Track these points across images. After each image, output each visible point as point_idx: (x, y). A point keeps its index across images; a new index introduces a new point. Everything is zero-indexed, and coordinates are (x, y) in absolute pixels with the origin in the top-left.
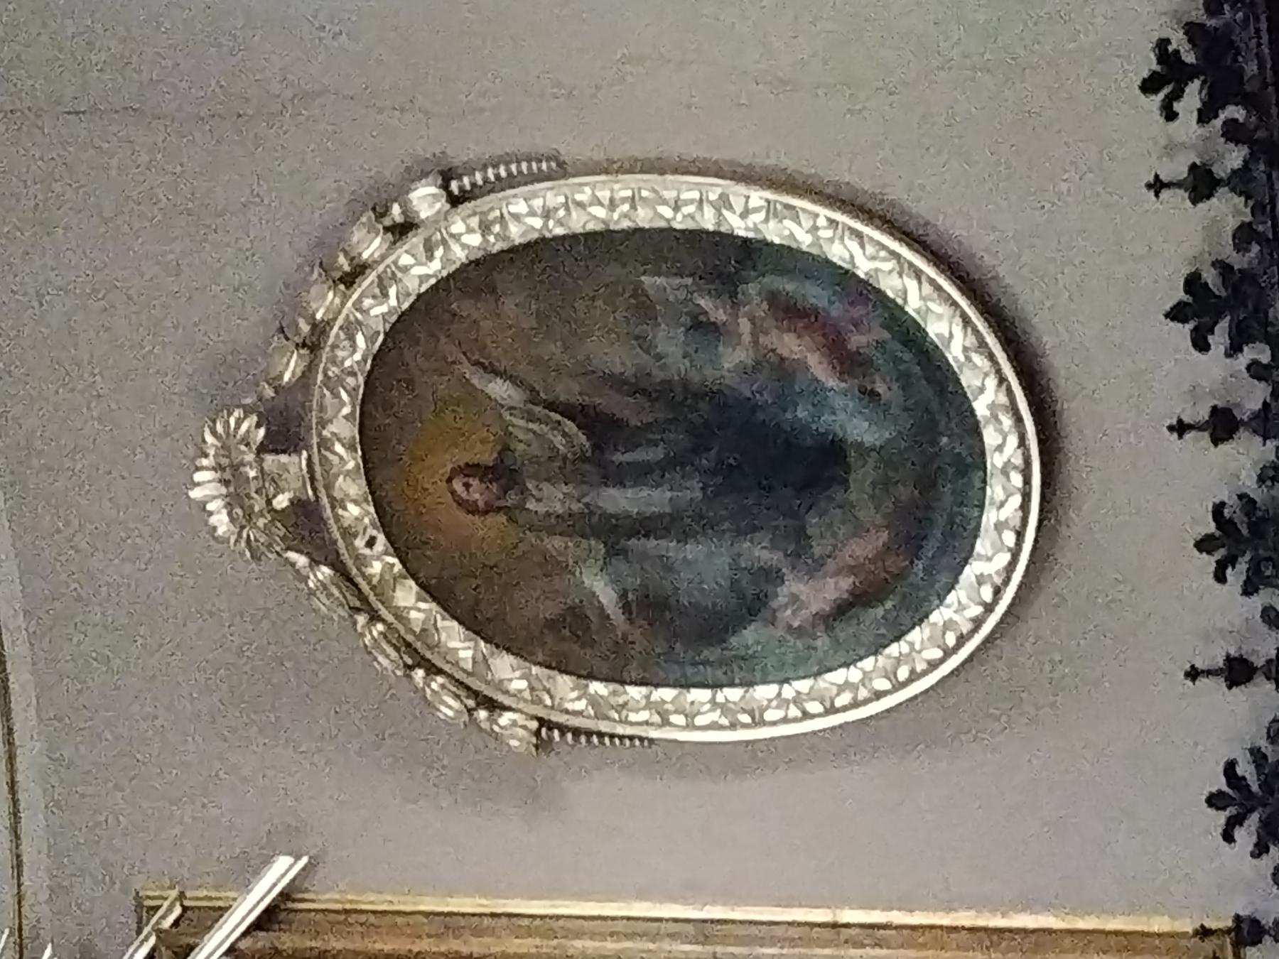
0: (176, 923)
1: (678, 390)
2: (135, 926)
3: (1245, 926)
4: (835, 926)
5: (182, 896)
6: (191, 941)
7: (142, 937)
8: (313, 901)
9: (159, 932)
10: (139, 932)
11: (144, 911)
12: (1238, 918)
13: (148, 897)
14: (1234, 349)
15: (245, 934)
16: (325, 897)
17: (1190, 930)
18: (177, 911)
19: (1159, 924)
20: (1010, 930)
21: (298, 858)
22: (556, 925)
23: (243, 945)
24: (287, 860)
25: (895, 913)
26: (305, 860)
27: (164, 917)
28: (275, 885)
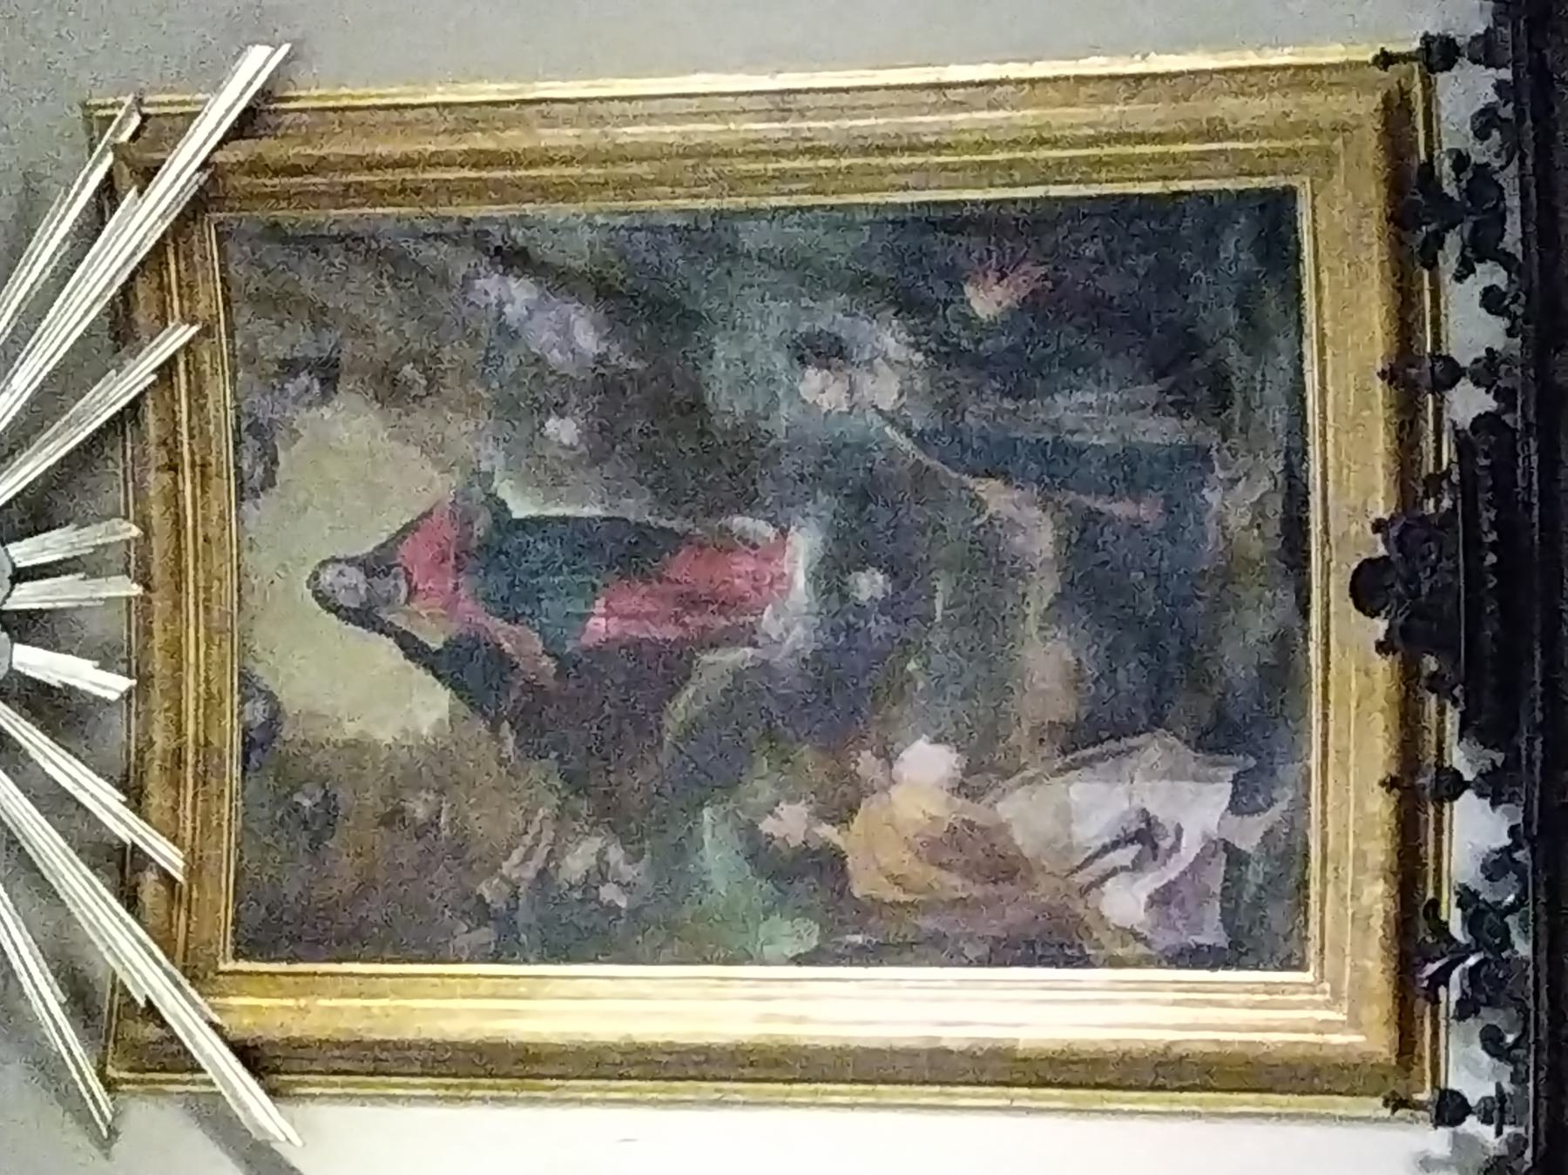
0: (135, 136)
1: (742, 506)
2: (85, 140)
3: (1434, 46)
4: (939, 87)
5: (139, 102)
6: (158, 156)
7: (95, 155)
8: (297, 99)
9: (116, 148)
10: (92, 149)
11: (96, 123)
12: (1426, 39)
13: (100, 107)
14: (1461, 161)
15: (220, 145)
16: (310, 93)
17: (1369, 58)
18: (136, 120)
19: (1333, 53)
20: (1154, 76)
21: (277, 47)
22: (599, 108)
23: (219, 157)
24: (267, 50)
25: (1011, 65)
26: (285, 48)
27: (119, 130)
28: (250, 84)
